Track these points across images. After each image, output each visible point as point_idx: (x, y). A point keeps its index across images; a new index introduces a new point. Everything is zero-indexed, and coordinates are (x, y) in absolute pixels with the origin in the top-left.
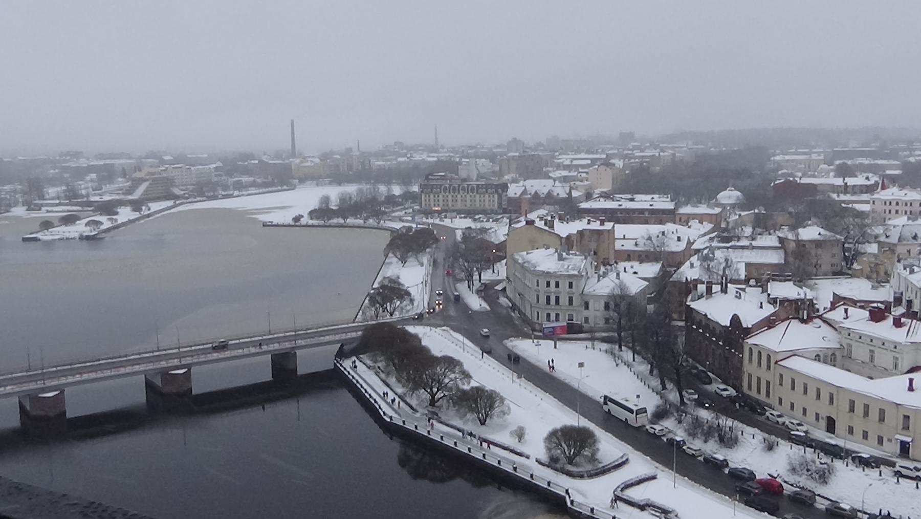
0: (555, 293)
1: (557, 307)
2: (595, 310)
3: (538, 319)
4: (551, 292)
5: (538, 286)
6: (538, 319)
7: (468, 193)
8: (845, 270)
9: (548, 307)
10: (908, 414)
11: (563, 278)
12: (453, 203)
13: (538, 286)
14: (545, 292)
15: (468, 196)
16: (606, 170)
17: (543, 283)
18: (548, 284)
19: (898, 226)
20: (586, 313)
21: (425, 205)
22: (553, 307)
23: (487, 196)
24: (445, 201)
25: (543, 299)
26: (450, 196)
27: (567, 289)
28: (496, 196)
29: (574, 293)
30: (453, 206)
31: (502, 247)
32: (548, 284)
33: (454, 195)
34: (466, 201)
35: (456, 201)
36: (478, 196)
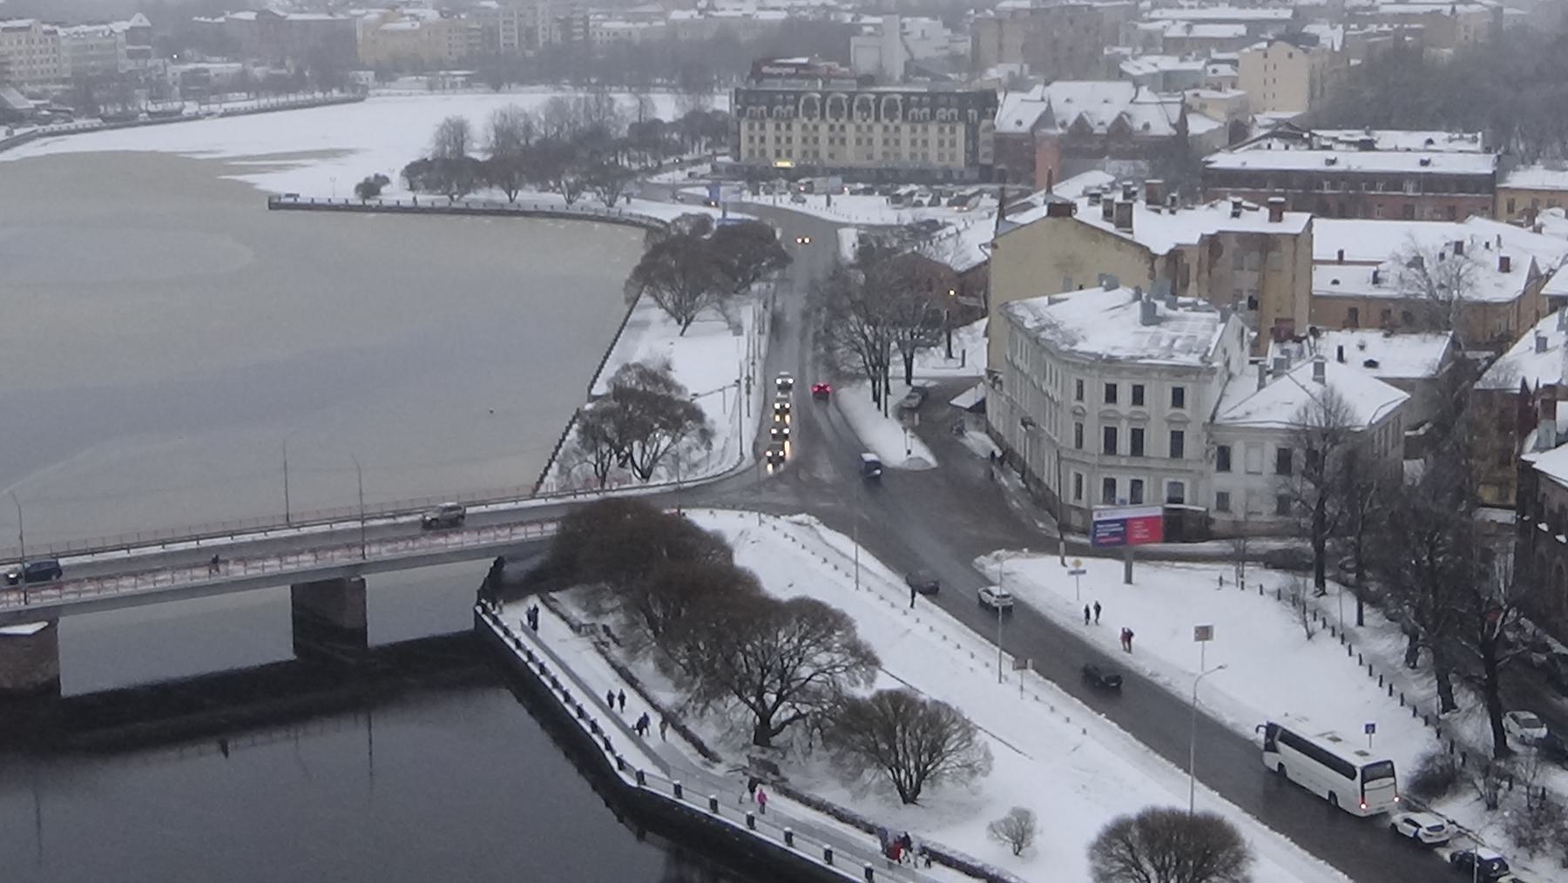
0: (1131, 419)
1: (1137, 462)
2: (1249, 473)
3: (1079, 495)
4: (1118, 418)
5: (1080, 397)
6: (1079, 495)
9: (1110, 460)
13: (1080, 397)
14: (1103, 417)
16: (1290, 55)
18: (1111, 394)
20: (1221, 481)
21: (751, 152)
22: (1124, 462)
25: (1094, 440)
27: (1169, 411)
28: (961, 129)
29: (1186, 422)
30: (831, 156)
32: (1111, 394)
33: (864, 128)
35: (843, 141)
36: (906, 128)
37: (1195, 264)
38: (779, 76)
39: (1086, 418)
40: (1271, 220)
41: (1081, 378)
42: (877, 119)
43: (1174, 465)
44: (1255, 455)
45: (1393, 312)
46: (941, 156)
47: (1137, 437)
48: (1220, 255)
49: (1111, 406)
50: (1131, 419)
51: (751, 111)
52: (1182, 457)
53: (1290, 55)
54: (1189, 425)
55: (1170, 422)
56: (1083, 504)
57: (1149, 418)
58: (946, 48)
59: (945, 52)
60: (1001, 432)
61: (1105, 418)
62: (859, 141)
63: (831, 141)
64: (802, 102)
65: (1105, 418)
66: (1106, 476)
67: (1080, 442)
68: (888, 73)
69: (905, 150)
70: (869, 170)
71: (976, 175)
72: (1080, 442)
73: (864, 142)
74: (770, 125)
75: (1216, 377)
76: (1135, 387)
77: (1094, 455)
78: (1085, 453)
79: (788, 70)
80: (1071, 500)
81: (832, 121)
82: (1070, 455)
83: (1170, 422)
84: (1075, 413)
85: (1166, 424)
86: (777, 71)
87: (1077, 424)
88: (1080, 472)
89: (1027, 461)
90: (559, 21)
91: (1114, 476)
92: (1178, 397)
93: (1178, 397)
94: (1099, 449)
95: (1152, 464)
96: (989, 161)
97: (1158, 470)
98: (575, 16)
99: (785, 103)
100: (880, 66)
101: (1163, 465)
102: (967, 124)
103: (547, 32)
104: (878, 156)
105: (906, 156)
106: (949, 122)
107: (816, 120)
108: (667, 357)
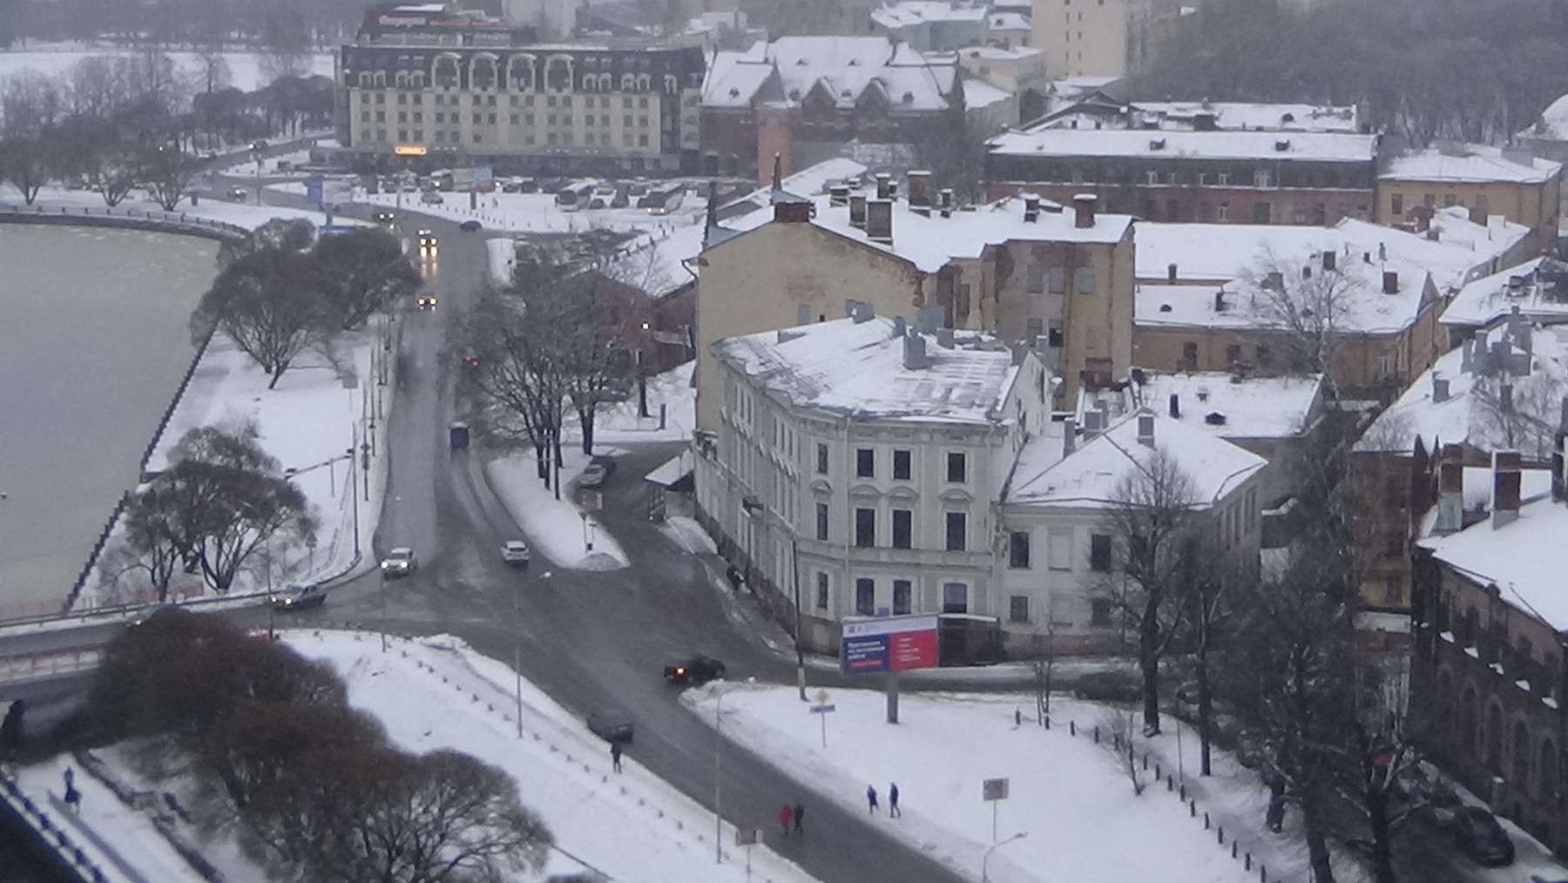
0: (893, 498)
1: (903, 557)
2: (1052, 569)
3: (823, 604)
4: (877, 496)
5: (823, 468)
6: (823, 604)
13: (823, 468)
14: (853, 496)
15: (540, 101)
17: (843, 458)
18: (866, 464)
20: (1017, 581)
22: (884, 557)
23: (616, 101)
25: (843, 527)
26: (466, 101)
27: (944, 486)
28: (655, 102)
30: (477, 139)
32: (866, 464)
34: (530, 119)
35: (492, 119)
36: (579, 101)
41: (823, 442)
43: (954, 559)
46: (628, 138)
47: (902, 523)
49: (865, 480)
50: (893, 498)
60: (716, 517)
62: (514, 119)
63: (477, 118)
65: (857, 497)
66: (860, 576)
73: (522, 120)
80: (814, 610)
85: (941, 504)
86: (401, 21)
88: (826, 572)
91: (871, 577)
92: (956, 468)
93: (956, 468)
95: (922, 559)
104: (541, 139)
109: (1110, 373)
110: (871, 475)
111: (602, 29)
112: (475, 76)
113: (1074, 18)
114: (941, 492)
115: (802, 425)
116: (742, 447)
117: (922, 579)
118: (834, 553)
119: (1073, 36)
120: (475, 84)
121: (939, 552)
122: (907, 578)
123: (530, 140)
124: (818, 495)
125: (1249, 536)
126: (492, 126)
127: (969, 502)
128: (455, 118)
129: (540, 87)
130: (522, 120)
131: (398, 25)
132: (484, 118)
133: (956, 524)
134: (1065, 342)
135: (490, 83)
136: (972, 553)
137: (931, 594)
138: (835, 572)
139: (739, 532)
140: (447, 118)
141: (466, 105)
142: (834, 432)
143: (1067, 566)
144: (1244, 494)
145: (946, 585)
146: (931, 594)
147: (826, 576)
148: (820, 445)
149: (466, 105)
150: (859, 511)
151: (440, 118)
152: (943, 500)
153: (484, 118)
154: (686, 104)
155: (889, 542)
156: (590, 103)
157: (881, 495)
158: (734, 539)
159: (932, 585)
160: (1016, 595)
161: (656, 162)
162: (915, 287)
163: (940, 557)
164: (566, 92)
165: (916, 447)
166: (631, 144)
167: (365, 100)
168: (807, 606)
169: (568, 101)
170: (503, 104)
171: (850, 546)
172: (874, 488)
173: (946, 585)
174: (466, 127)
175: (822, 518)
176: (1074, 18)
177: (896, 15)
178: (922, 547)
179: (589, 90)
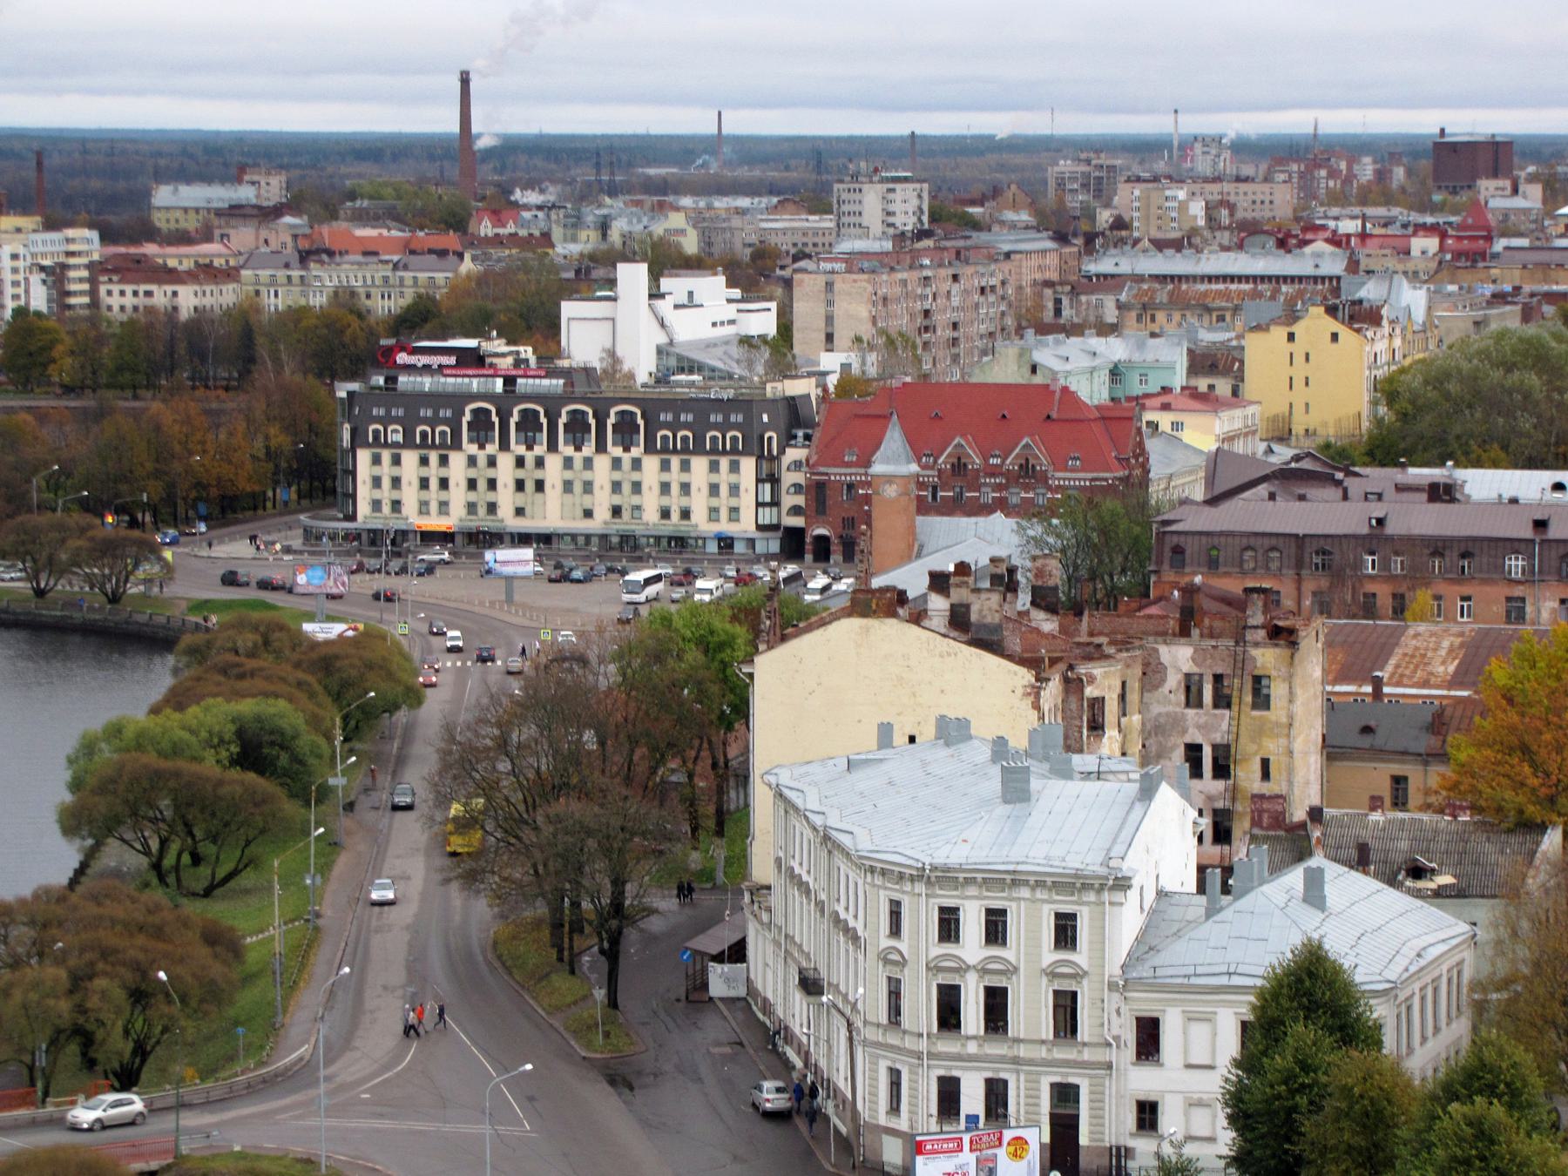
0: (984, 972)
1: (996, 1048)
2: (1189, 1066)
3: (895, 1108)
4: (963, 969)
5: (895, 930)
6: (895, 1108)
7: (553, 447)
8: (1470, 544)
9: (947, 1046)
10: (1329, 336)
11: (1025, 892)
12: (520, 500)
13: (895, 930)
14: (934, 968)
15: (602, 463)
16: (1335, 337)
17: (922, 917)
18: (949, 925)
19: (420, 575)
20: (1143, 1081)
21: (376, 505)
22: (972, 1048)
23: (699, 464)
24: (482, 485)
25: (921, 1008)
26: (506, 462)
27: (1049, 955)
28: (748, 465)
29: (1078, 976)
30: (520, 512)
31: (324, 793)
32: (949, 925)
33: (530, 457)
34: (588, 487)
35: (540, 486)
36: (651, 464)
37: (1115, 696)
38: (427, 368)
39: (906, 971)
40: (967, 607)
41: (896, 896)
42: (504, 446)
43: (1063, 1053)
44: (1199, 1031)
45: (177, 716)
46: (713, 513)
47: (996, 1006)
48: (1157, 687)
49: (949, 948)
50: (984, 972)
51: (376, 432)
52: (1005, 1031)
53: (1335, 337)
54: (1085, 982)
55: (1053, 975)
56: (903, 1124)
57: (1016, 969)
58: (732, 322)
59: (729, 330)
60: (770, 996)
61: (940, 969)
62: (568, 486)
63: (520, 485)
64: (467, 418)
65: (940, 969)
66: (942, 1072)
67: (895, 1010)
68: (626, 367)
69: (651, 503)
70: (588, 537)
71: (775, 547)
72: (895, 1010)
73: (578, 487)
74: (410, 458)
75: (1133, 895)
76: (990, 912)
77: (921, 1035)
78: (1018, 1041)
79: (435, 361)
80: (883, 1119)
81: (521, 450)
82: (871, 1034)
83: (1053, 975)
84: (887, 962)
85: (1045, 980)
86: (423, 360)
87: (889, 979)
88: (898, 1066)
89: (812, 1050)
90: (43, 269)
91: (955, 1073)
92: (1065, 933)
93: (1065, 933)
94: (929, 1025)
95: (1023, 1051)
96: (798, 522)
97: (1031, 1062)
98: (72, 261)
99: (674, 426)
100: (612, 353)
101: (1043, 1052)
102: (760, 457)
103: (21, 291)
104: (602, 515)
105: (651, 515)
106: (417, 447)
107: (491, 448)
108: (1316, 936)
109: (1283, 813)
110: (957, 940)
111: (691, 372)
112: (566, 431)
113: (1299, 359)
114: (1044, 965)
115: (869, 875)
116: (802, 903)
117: (1022, 1077)
118: (909, 1043)
119: (1299, 383)
120: (471, 441)
121: (1043, 1042)
122: (1003, 1075)
123: (588, 514)
124: (889, 967)
125: (1454, 1025)
126: (539, 495)
127: (1082, 977)
128: (492, 484)
129: (504, 446)
130: (578, 487)
131: (420, 365)
132: (530, 486)
133: (1066, 1011)
134: (1232, 772)
135: (490, 440)
136: (1084, 1044)
137: (1033, 1096)
138: (911, 1065)
139: (797, 1017)
140: (482, 485)
141: (505, 471)
142: (909, 884)
143: (1207, 1062)
144: (1444, 972)
145: (1053, 1085)
146: (1033, 1096)
147: (898, 1072)
148: (891, 901)
149: (505, 471)
150: (940, 987)
151: (472, 484)
152: (1047, 975)
153: (530, 486)
154: (788, 469)
155: (978, 1028)
156: (665, 466)
157: (969, 967)
158: (791, 1026)
159: (1034, 1083)
160: (1142, 1098)
161: (751, 542)
162: (1032, 698)
163: (1044, 1048)
164: (636, 451)
165: (1014, 905)
166: (718, 520)
167: (376, 460)
168: (875, 1111)
169: (637, 464)
170: (553, 470)
171: (928, 1035)
172: (960, 958)
173: (1053, 1085)
174: (506, 499)
175: (893, 996)
176: (1299, 359)
177: (1066, 355)
178: (1022, 1036)
179: (665, 450)
